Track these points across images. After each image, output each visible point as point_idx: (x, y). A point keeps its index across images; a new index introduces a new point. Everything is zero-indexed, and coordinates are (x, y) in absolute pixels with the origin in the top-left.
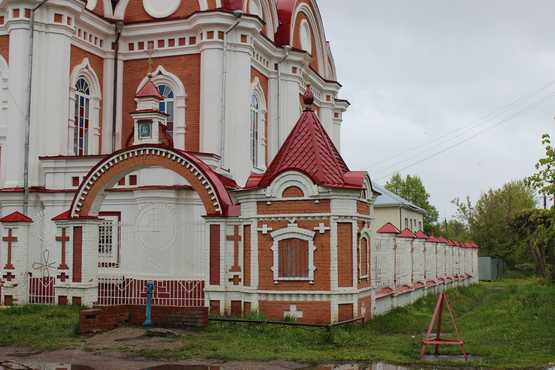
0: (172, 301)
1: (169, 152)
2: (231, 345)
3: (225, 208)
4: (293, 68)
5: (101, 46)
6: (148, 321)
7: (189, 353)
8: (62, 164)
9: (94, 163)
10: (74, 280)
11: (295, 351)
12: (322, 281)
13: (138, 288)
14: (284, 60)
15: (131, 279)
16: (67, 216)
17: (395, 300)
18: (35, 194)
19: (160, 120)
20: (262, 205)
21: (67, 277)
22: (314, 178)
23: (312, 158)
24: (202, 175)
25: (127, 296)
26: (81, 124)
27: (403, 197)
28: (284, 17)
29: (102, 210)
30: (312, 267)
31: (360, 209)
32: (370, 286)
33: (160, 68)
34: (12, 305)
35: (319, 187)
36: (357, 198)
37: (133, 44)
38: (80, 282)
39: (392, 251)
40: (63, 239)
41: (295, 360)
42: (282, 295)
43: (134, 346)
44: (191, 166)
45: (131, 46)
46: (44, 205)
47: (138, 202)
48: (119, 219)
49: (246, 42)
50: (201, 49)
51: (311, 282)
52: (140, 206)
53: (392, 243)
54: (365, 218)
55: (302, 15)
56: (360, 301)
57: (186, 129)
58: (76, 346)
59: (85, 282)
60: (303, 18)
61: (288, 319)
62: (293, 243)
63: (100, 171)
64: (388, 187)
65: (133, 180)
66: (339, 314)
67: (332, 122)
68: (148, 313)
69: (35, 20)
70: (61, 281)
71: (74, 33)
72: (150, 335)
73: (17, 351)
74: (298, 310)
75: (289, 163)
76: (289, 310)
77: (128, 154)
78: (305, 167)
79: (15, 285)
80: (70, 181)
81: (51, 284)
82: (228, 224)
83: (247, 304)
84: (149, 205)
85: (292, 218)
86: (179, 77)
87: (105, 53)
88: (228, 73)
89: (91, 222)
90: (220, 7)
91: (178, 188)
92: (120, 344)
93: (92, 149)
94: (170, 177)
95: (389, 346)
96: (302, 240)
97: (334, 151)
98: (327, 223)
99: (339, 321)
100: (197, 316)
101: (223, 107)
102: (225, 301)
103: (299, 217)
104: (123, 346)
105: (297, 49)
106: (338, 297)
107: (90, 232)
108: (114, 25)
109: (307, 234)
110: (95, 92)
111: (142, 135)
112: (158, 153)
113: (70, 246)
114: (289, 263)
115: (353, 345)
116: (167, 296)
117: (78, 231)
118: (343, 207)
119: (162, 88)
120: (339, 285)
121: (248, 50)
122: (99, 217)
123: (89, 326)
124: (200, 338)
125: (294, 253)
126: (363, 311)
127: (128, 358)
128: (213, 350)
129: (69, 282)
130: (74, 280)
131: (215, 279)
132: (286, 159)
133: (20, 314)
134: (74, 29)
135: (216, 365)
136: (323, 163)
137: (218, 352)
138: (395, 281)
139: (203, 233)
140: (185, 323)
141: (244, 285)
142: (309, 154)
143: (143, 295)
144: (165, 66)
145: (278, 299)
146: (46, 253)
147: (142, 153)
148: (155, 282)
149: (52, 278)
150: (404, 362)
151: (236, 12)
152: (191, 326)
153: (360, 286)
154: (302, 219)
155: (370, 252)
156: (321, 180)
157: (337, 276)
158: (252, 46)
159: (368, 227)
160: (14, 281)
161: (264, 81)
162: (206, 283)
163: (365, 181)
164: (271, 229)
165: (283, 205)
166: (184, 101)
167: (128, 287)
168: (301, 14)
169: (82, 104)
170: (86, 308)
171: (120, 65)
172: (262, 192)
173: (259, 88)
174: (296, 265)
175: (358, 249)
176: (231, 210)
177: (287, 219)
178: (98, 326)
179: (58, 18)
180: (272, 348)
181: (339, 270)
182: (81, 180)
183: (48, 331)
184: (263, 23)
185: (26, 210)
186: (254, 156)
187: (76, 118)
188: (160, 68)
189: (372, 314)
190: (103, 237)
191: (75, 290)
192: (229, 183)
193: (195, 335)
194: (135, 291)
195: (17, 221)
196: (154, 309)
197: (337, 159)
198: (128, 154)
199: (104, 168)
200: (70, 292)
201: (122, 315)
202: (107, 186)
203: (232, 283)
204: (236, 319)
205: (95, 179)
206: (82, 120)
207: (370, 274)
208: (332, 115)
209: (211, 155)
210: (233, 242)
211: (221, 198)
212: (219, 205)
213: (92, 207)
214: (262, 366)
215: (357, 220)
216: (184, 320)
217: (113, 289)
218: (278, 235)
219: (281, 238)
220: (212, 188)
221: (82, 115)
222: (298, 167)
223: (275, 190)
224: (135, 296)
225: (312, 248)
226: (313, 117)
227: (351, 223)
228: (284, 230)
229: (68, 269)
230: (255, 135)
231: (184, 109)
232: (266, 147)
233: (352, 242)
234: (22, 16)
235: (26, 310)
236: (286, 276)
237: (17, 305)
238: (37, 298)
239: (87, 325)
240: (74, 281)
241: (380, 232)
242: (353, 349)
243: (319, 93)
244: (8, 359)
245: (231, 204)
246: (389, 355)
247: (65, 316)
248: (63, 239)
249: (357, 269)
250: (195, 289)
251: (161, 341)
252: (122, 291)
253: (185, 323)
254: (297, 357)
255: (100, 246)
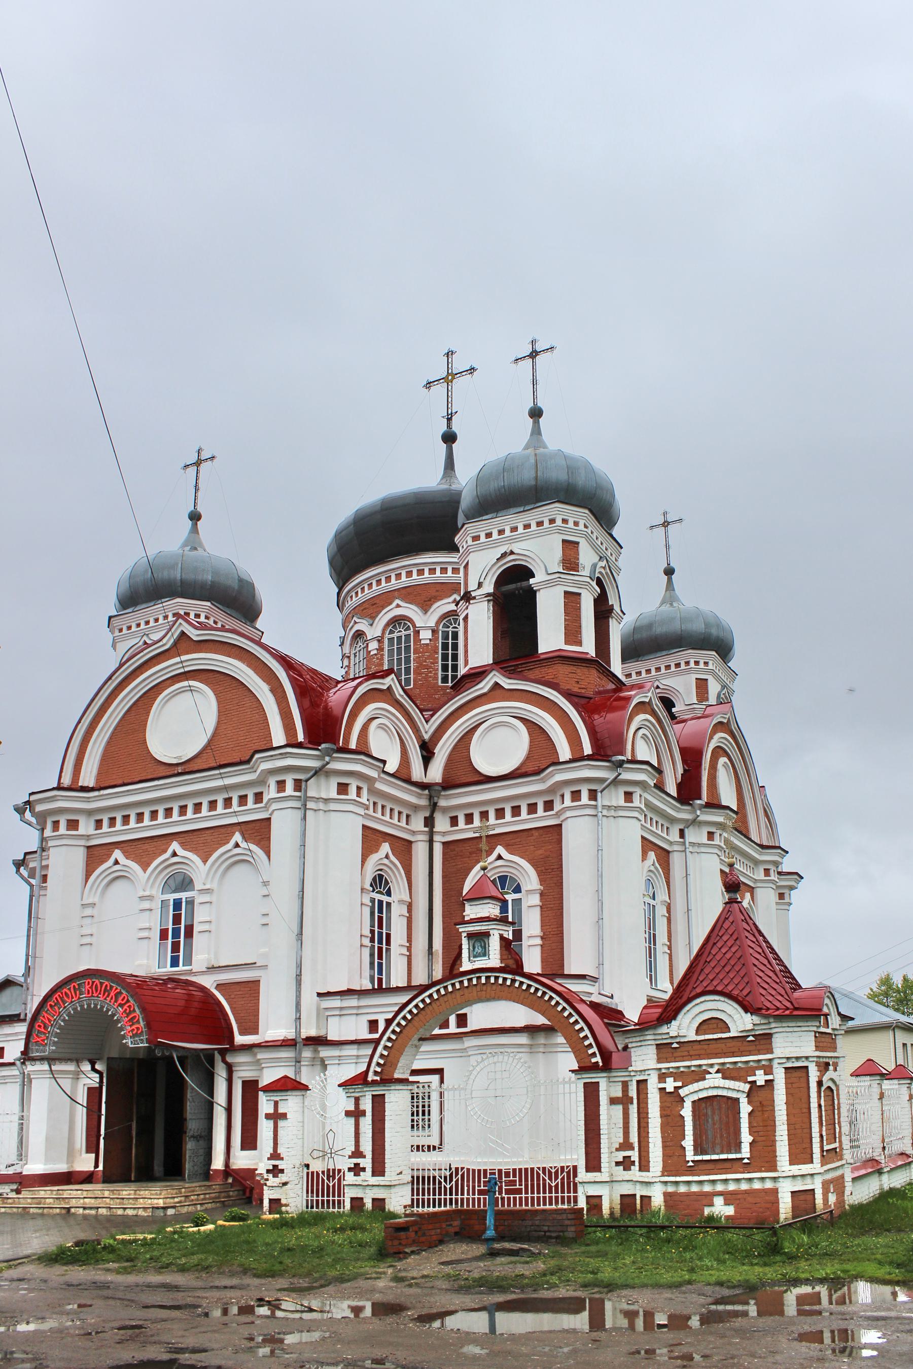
0: (524, 1201)
1: (517, 978)
2: (619, 1263)
3: (606, 1055)
4: (709, 833)
5: (407, 824)
6: (490, 1233)
7: (554, 1279)
8: (353, 1002)
9: (404, 999)
10: (374, 1173)
11: (722, 1268)
12: (764, 1157)
13: (474, 1182)
14: (695, 822)
15: (462, 1168)
16: (361, 1080)
17: (885, 1177)
18: (311, 1048)
19: (501, 932)
20: (665, 1050)
21: (364, 1169)
22: (746, 1003)
23: (742, 973)
24: (569, 1010)
25: (457, 1194)
26: (379, 941)
27: (897, 1010)
28: (691, 757)
29: (417, 1066)
30: (746, 1138)
31: (821, 1044)
32: (841, 1159)
33: (500, 850)
34: (280, 1213)
35: (754, 1017)
36: (815, 1029)
37: (457, 817)
38: (384, 1176)
39: (878, 1103)
40: (356, 1114)
41: (720, 1284)
42: (701, 1182)
43: (469, 1272)
44: (551, 998)
45: (454, 821)
46: (326, 1063)
47: (470, 1053)
48: (442, 1081)
49: (632, 802)
50: (562, 818)
51: (746, 1161)
52: (473, 1060)
53: (876, 1091)
54: (829, 1057)
55: (719, 751)
56: (826, 1185)
57: (542, 938)
58: (381, 1273)
59: (390, 1176)
60: (721, 756)
61: (711, 1218)
62: (715, 1103)
63: (410, 1012)
64: (873, 996)
65: (462, 1020)
66: (793, 1207)
67: (774, 906)
68: (490, 1221)
69: (309, 794)
70: (355, 1175)
71: (367, 809)
72: (493, 1254)
73: (292, 1284)
74: (727, 1203)
75: (705, 984)
76: (712, 1205)
77: (453, 985)
78: (730, 988)
79: (285, 1184)
80: (365, 1027)
81: (339, 1180)
82: (612, 1080)
83: (646, 1199)
84: (488, 1057)
85: (712, 1065)
86: (529, 861)
87: (414, 833)
88: (605, 847)
89: (397, 1087)
90: (590, 753)
91: (531, 1030)
92: (448, 1269)
93: (398, 978)
94: (518, 1014)
95: (873, 1254)
96: (729, 1098)
97: (775, 959)
98: (768, 1070)
99: (793, 1218)
100: (567, 1222)
101: (600, 902)
102: (611, 1196)
103: (723, 1064)
104: (452, 1272)
105: (714, 805)
106: (788, 1181)
107: (397, 1102)
108: (427, 792)
109: (737, 1089)
110: (400, 892)
111: (473, 955)
112: (500, 981)
113: (366, 1124)
114: (709, 1133)
115: (815, 1255)
116: (519, 1191)
117: (379, 1102)
118: (793, 1043)
119: (503, 879)
120: (792, 1163)
121: (636, 814)
122: (412, 1079)
123: (400, 1244)
124: (572, 1255)
125: (716, 1118)
126: (832, 1198)
127: (459, 1290)
128: (593, 1273)
129: (367, 1176)
130: (374, 1173)
131: (593, 1164)
132: (701, 978)
133: (293, 1228)
134: (367, 803)
135: (597, 1296)
136: (759, 980)
137: (600, 1275)
138: (884, 1148)
139: (573, 1095)
140: (548, 1234)
141: (640, 1170)
142: (737, 968)
143: (481, 1192)
144: (508, 847)
145: (695, 1188)
146: (331, 1135)
147: (475, 982)
148: (500, 1171)
149: (339, 1171)
150: (897, 1279)
151: (614, 758)
152: (557, 1238)
153: (824, 1160)
154: (728, 1066)
155: (839, 1108)
156: (756, 1006)
157: (787, 1148)
158: (643, 806)
159: (835, 1070)
160: (283, 1178)
161: (664, 856)
162: (579, 1170)
163: (827, 1001)
164: (679, 1084)
165: (697, 1047)
166: (538, 896)
167: (457, 1182)
168: (719, 750)
169: (380, 911)
170: (394, 1216)
171: (438, 849)
172: (664, 1029)
173: (656, 868)
174: (722, 1136)
175: (820, 1106)
176: (615, 1057)
177: (704, 1068)
178: (414, 1242)
179: (343, 788)
180: (685, 1266)
181: (789, 1140)
182: (381, 1026)
183: (338, 1253)
184: (659, 771)
185: (298, 1072)
186: (651, 971)
187: (372, 932)
188: (500, 850)
189: (847, 1202)
190: (418, 1107)
191: (375, 1190)
192: (610, 1015)
193: (564, 1250)
194: (468, 1186)
195: (287, 1090)
196: (498, 1214)
197: (781, 971)
198: (453, 985)
199: (416, 1006)
200: (367, 1191)
201: (451, 1225)
202: (422, 1033)
203: (621, 1168)
204: (628, 1223)
205: (403, 1023)
206: (380, 934)
207: (840, 1141)
208: (773, 896)
209: (582, 977)
210: (620, 1107)
211: (600, 1039)
212: (597, 1053)
213: (400, 1065)
214: (669, 1295)
215: (817, 1062)
216: (546, 1228)
217: (434, 1183)
218: (692, 1092)
219: (695, 1097)
220: (585, 1028)
221: (380, 927)
222: (719, 988)
223: (685, 1026)
224: (468, 1194)
225: (745, 1109)
226: (741, 911)
227: (807, 1067)
228: (701, 1085)
229: (364, 1157)
230: (652, 939)
231: (538, 909)
232: (670, 956)
233: (809, 1096)
234: (289, 790)
235: (302, 1220)
236: (707, 1154)
237: (287, 1212)
238: (317, 1201)
239: (396, 1242)
240: (373, 1175)
241: (856, 1074)
242: (815, 1261)
243: (752, 866)
244: (279, 1295)
245: (615, 1050)
246: (871, 1269)
247: (363, 1229)
248: (356, 1114)
249: (818, 1135)
250: (563, 1179)
251: (511, 1263)
252: (448, 1187)
253: (548, 1234)
254: (724, 1278)
255: (413, 1121)
